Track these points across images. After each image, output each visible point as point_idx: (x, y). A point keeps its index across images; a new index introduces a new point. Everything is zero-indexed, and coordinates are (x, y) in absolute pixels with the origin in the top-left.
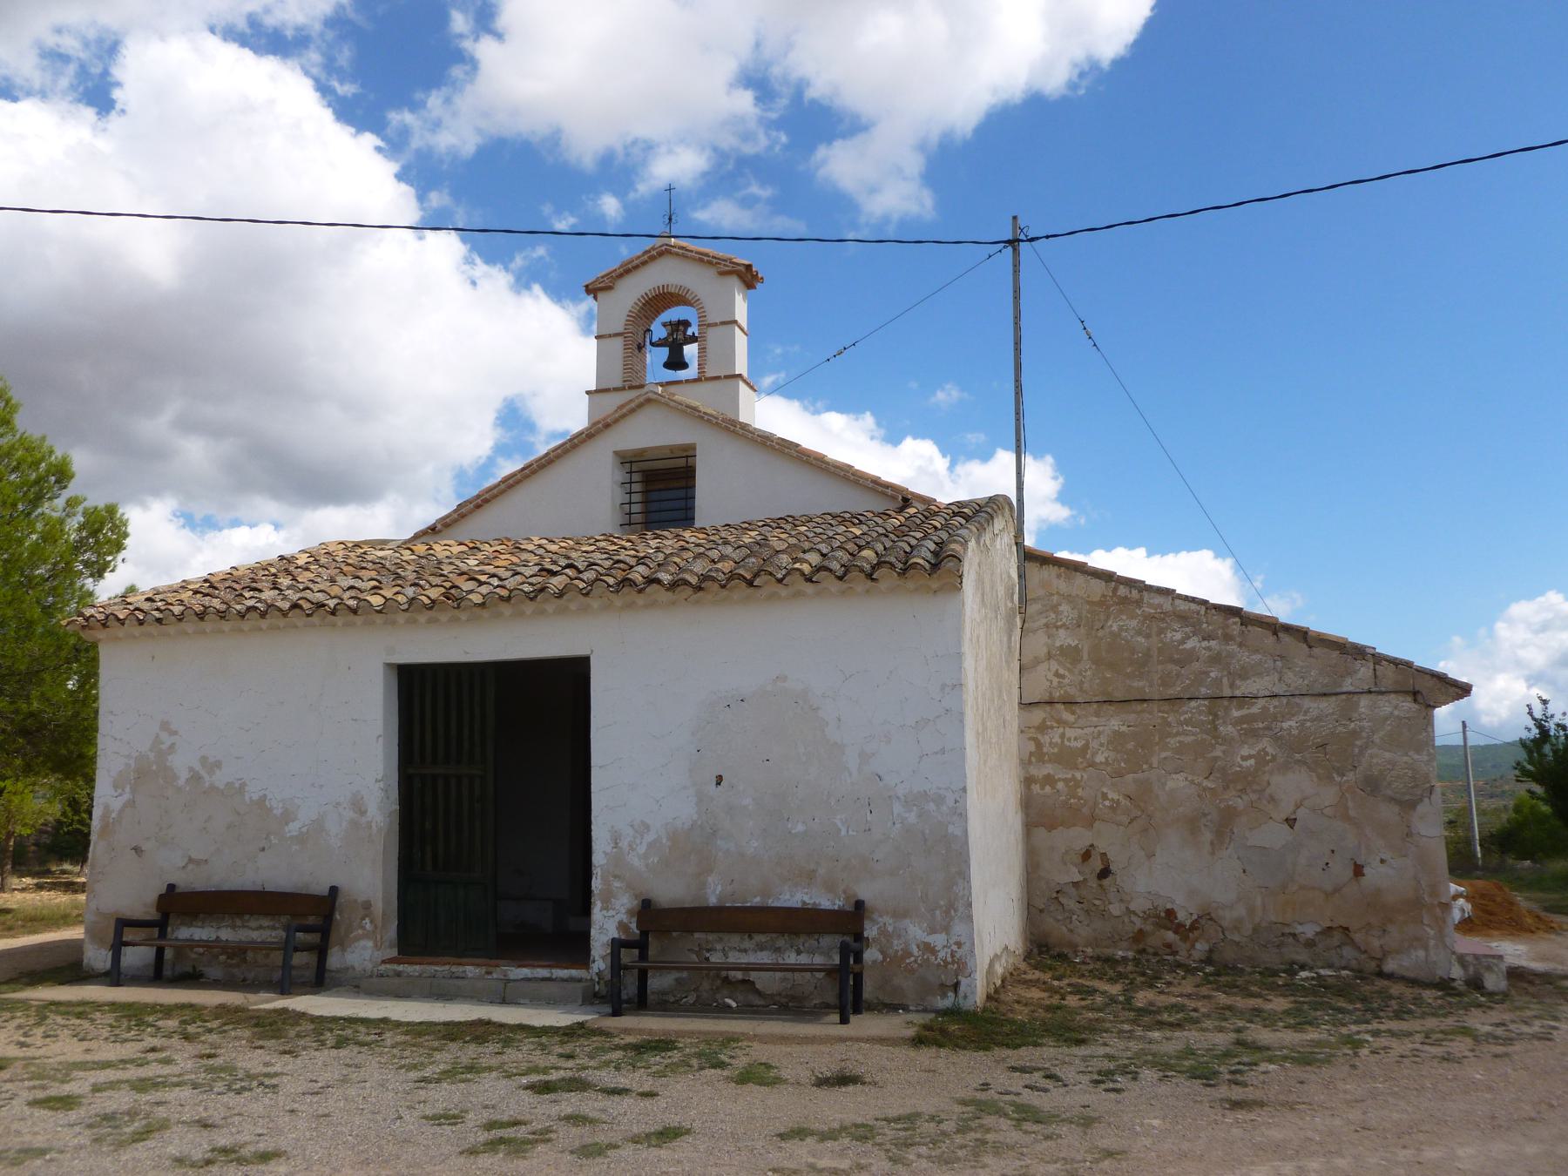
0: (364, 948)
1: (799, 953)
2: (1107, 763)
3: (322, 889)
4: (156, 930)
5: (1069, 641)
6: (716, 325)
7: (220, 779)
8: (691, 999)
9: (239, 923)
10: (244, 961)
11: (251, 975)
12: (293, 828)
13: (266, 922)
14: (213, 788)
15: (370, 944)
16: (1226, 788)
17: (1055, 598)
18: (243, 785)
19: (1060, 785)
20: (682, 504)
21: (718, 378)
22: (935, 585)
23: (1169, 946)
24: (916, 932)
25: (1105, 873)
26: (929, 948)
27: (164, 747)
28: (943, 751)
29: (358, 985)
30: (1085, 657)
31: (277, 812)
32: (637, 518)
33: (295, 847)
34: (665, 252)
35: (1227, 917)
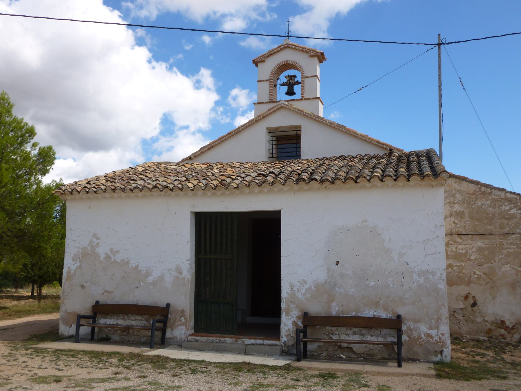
0: (181, 329)
1: (372, 336)
2: (476, 260)
3: (162, 303)
4: (91, 321)
5: (459, 209)
6: (308, 77)
7: (118, 258)
8: (325, 354)
9: (126, 317)
11: (131, 339)
12: (150, 279)
13: (138, 317)
14: (115, 261)
15: (184, 328)
17: (454, 191)
18: (129, 261)
19: (455, 268)
20: (295, 150)
21: (310, 99)
22: (434, 183)
23: (502, 335)
24: (423, 329)
25: (474, 305)
26: (429, 336)
27: (94, 244)
28: (435, 253)
29: (180, 345)
30: (467, 215)
32: (274, 155)
33: (151, 287)
34: (287, 47)
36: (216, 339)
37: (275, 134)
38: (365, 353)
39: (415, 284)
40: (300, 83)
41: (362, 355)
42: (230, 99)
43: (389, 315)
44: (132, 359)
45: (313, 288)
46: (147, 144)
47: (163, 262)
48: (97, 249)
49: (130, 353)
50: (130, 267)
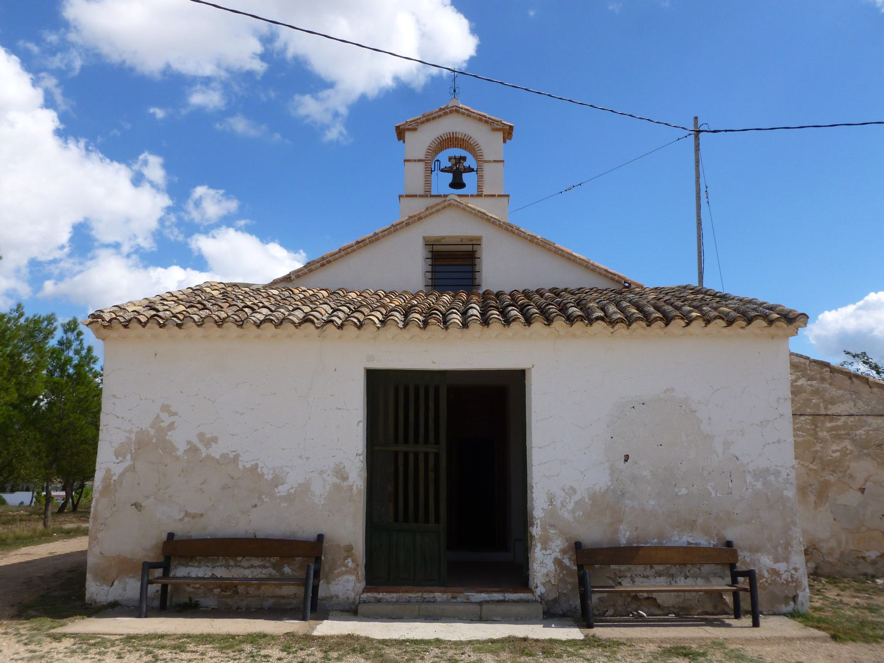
7: (216, 451)
9: (232, 563)
10: (236, 592)
11: (244, 604)
12: (282, 490)
13: (256, 562)
14: (209, 457)
15: (352, 578)
16: (823, 469)
18: (237, 456)
26: (775, 572)
28: (779, 441)
31: (269, 477)
35: (825, 547)
36: (416, 595)
37: (436, 248)
39: (750, 490)
40: (473, 170)
41: (672, 609)
42: (190, 206)
46: (37, 271)
47: (308, 458)
48: (169, 433)
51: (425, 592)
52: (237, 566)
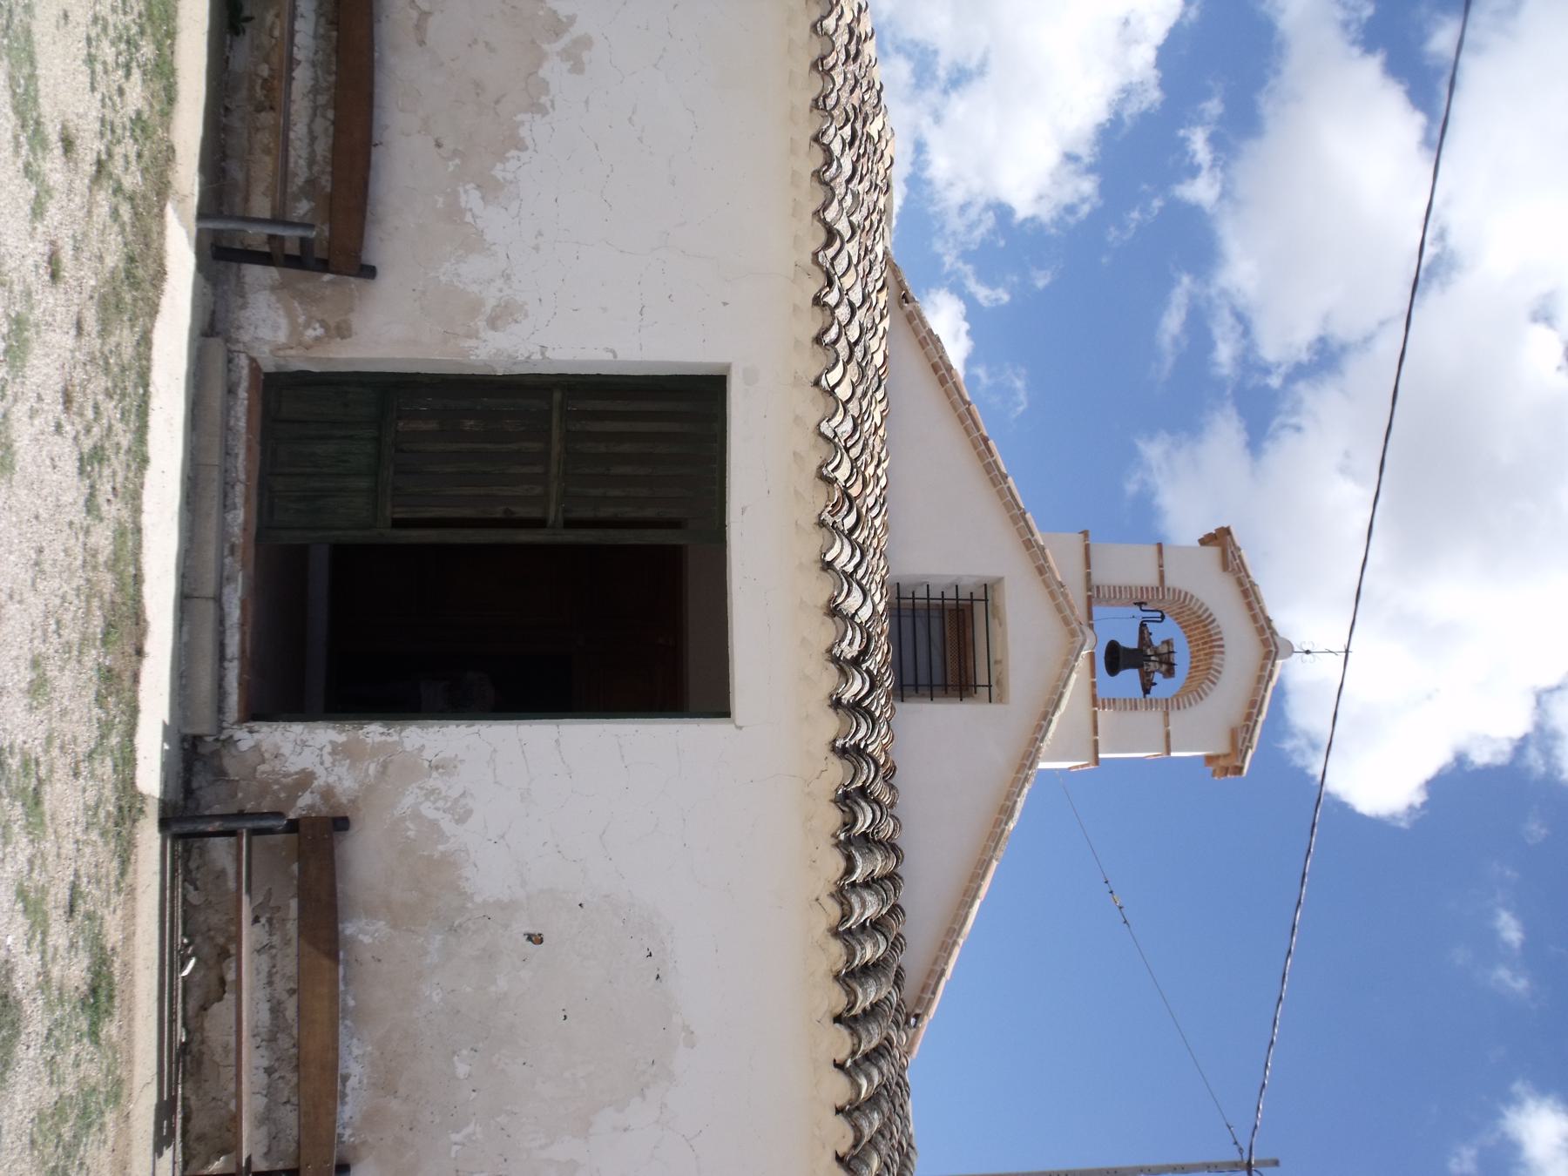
6: (1167, 724)
7: (554, 71)
9: (322, 99)
10: (259, 109)
12: (471, 198)
13: (322, 147)
14: (541, 58)
15: (282, 337)
18: (541, 110)
20: (923, 679)
29: (212, 327)
31: (498, 172)
37: (979, 608)
38: (204, 1048)
40: (1146, 691)
43: (348, 1132)
44: (144, 171)
45: (441, 848)
47: (537, 248)
49: (171, 149)
50: (519, 117)
51: (247, 487)
52: (315, 109)
